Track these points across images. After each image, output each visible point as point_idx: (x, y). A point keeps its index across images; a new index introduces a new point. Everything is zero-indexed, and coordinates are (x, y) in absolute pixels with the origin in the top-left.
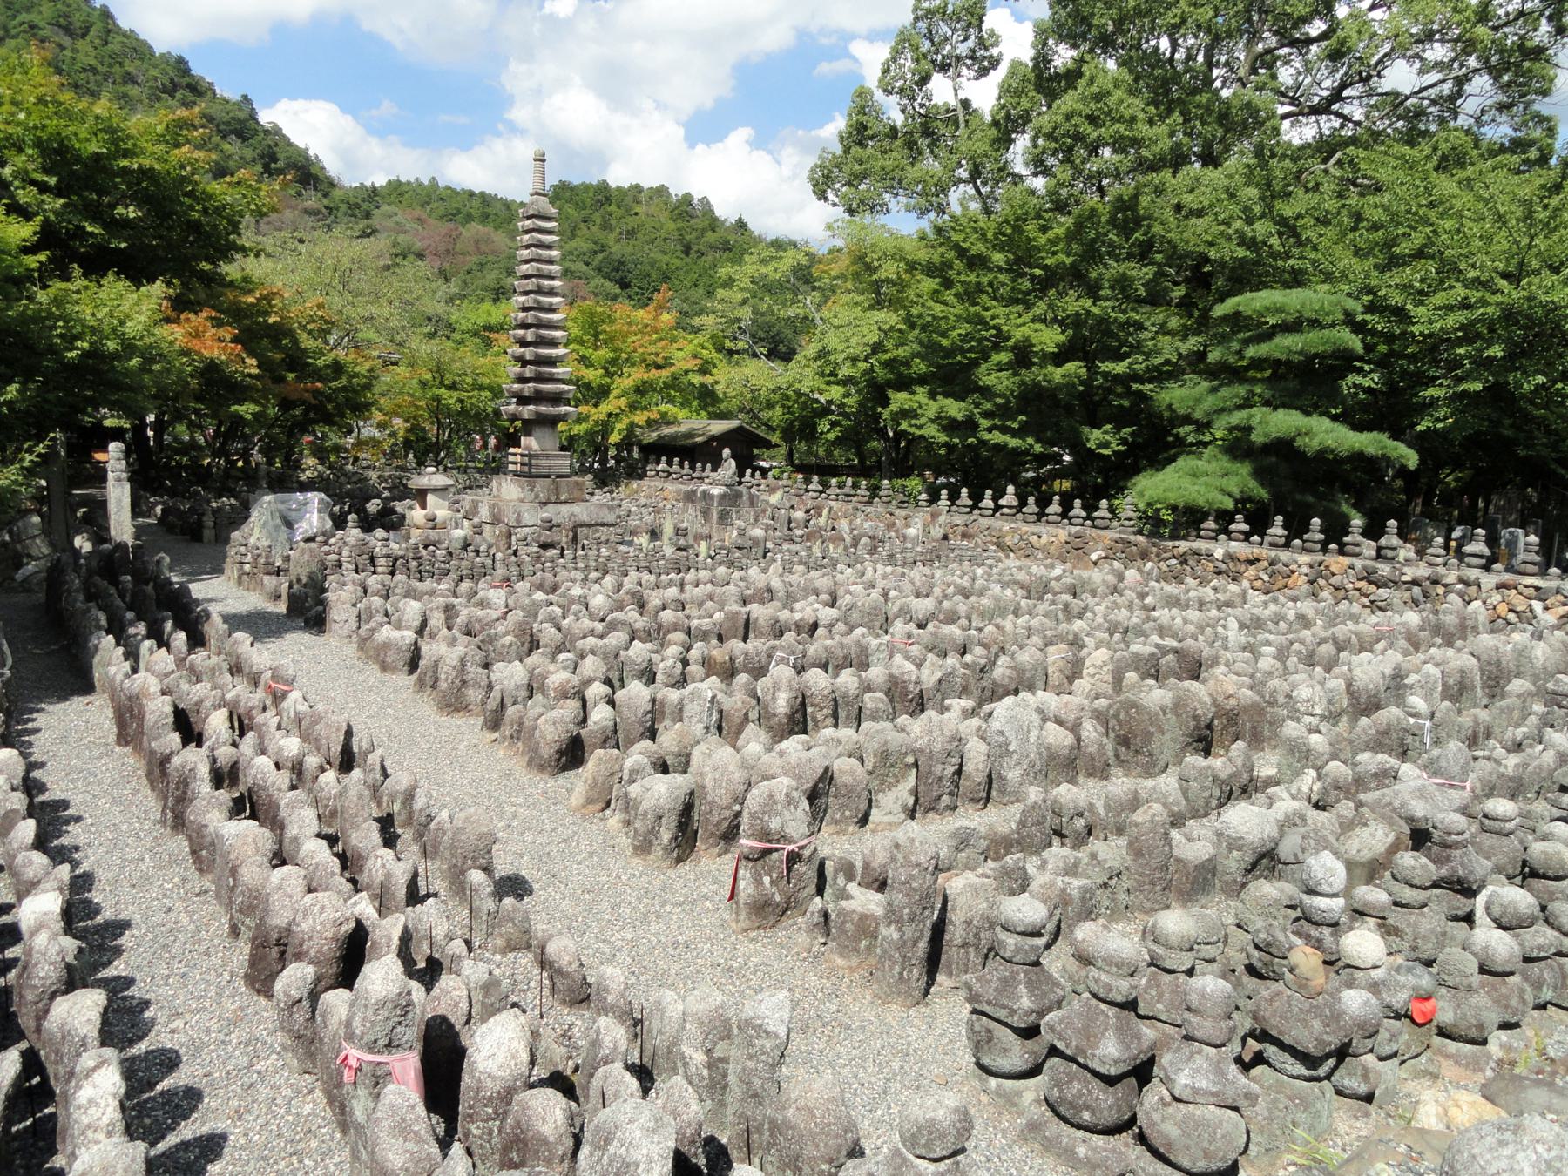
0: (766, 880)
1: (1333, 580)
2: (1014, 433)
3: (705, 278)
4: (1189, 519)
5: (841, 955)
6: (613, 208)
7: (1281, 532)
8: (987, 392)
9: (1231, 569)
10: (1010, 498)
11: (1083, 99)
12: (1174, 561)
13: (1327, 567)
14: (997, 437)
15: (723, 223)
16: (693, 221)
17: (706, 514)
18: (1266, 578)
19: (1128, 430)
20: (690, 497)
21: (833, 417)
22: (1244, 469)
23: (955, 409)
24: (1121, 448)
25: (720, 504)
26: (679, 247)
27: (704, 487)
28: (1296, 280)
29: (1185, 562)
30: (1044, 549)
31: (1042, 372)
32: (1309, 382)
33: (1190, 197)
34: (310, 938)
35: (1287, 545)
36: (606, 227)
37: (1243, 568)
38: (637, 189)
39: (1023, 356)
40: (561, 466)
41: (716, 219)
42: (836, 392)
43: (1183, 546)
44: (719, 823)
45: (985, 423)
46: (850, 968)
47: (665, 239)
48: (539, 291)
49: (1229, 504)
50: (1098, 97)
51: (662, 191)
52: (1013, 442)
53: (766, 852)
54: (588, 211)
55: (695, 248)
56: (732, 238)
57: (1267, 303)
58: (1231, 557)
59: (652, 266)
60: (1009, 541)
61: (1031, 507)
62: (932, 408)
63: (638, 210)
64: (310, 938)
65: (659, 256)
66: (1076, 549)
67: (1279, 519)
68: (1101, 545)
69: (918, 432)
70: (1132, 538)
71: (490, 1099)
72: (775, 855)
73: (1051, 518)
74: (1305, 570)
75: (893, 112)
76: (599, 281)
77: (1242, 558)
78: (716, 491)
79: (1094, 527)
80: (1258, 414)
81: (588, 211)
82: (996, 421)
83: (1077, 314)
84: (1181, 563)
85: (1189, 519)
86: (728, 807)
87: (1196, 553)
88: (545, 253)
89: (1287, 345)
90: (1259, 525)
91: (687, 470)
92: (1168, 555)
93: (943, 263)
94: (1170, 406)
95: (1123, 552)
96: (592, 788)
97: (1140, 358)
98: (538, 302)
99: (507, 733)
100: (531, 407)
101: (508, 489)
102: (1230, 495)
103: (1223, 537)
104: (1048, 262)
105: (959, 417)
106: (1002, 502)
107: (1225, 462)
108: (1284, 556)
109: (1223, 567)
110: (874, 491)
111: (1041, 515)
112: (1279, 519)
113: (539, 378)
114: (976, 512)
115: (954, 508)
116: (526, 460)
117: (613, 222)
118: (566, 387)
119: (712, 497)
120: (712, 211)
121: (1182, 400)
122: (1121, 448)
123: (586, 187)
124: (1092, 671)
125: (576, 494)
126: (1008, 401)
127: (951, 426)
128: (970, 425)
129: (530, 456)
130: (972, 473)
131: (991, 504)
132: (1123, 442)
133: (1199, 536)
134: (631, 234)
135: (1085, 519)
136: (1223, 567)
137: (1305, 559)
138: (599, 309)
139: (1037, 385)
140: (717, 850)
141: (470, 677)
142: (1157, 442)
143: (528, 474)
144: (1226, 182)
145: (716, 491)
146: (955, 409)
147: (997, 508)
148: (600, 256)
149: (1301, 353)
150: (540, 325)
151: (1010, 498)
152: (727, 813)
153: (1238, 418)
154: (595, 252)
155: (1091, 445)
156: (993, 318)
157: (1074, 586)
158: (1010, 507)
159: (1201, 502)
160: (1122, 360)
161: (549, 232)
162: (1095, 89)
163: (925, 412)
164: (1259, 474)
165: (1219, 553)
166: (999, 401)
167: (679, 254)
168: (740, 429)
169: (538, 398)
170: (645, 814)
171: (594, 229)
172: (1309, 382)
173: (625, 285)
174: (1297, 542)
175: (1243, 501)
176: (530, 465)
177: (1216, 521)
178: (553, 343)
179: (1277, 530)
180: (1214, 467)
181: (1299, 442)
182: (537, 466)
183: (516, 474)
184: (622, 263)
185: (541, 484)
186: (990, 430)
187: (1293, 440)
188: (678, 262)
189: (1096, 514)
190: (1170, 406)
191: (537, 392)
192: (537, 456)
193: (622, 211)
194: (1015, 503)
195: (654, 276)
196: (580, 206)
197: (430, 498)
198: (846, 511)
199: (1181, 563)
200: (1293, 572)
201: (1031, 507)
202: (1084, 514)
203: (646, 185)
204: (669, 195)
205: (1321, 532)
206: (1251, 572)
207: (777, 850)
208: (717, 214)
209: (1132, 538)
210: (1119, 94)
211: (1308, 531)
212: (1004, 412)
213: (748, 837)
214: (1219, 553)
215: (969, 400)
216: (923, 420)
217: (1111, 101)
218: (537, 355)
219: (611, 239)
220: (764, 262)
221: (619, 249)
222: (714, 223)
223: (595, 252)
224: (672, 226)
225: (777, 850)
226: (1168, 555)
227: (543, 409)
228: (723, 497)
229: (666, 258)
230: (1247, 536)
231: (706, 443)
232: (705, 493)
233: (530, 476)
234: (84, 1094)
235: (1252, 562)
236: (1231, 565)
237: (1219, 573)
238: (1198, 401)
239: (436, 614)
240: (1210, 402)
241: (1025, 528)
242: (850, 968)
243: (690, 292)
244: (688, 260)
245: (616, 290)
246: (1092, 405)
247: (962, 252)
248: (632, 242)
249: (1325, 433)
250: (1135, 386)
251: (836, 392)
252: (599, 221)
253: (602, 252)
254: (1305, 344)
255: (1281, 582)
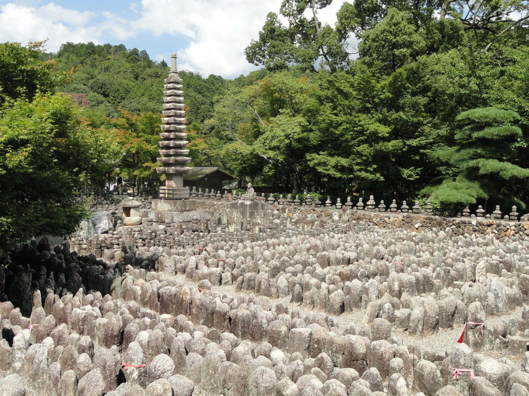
0: (476, 335)
1: (526, 232)
2: (371, 173)
3: (148, 91)
4: (451, 209)
5: (513, 355)
6: (96, 56)
7: (499, 212)
8: (359, 154)
9: (480, 229)
10: (371, 201)
11: (389, 24)
12: (454, 227)
13: (523, 227)
14: (363, 174)
15: (154, 63)
16: (139, 63)
17: (243, 213)
18: (496, 232)
19: (420, 169)
20: (234, 206)
21: (270, 165)
22: (476, 185)
23: (344, 162)
24: (418, 177)
25: (250, 209)
26: (132, 76)
27: (240, 201)
28: (485, 103)
29: (460, 227)
30: (393, 224)
31: (368, 141)
32: (499, 147)
33: (437, 67)
34: (385, 353)
35: (502, 218)
36: (93, 66)
37: (486, 228)
38: (108, 46)
39: (374, 138)
40: (186, 194)
41: (151, 61)
42: (271, 154)
43: (458, 220)
44: (432, 323)
45: (356, 168)
46: (517, 358)
47: (125, 72)
48: (176, 115)
49: (474, 201)
50: (395, 25)
51: (121, 48)
52: (371, 177)
53: (476, 325)
54: (83, 58)
55: (141, 76)
56: (159, 71)
57: (481, 114)
58: (479, 224)
59: (120, 85)
60: (375, 220)
61: (382, 205)
62: (333, 161)
63: (109, 57)
64: (385, 353)
65: (123, 81)
66: (407, 223)
67: (498, 207)
68: (419, 221)
69: (327, 172)
70: (434, 217)
71: (495, 380)
72: (478, 327)
73: (392, 209)
74: (513, 228)
75: (285, 23)
76: (91, 94)
77: (485, 224)
78: (248, 203)
79: (413, 212)
80: (481, 162)
81: (83, 58)
82: (363, 167)
83: (396, 119)
84: (457, 227)
85: (451, 209)
86: (435, 317)
87: (464, 223)
88: (178, 99)
89: (489, 132)
90: (489, 210)
91: (200, 192)
92: (451, 224)
93: (333, 96)
94: (438, 158)
95: (427, 224)
96: (370, 316)
97: (424, 138)
98: (175, 120)
99: (308, 302)
100: (173, 168)
101: (162, 206)
102: (473, 197)
103: (473, 215)
104: (382, 96)
105: (346, 165)
106: (368, 203)
107: (466, 183)
108: (503, 222)
109: (477, 228)
110: (276, 199)
111: (387, 208)
112: (498, 207)
113: (176, 155)
114: (355, 208)
115: (344, 206)
116: (171, 192)
117: (97, 63)
118: (188, 158)
119: (246, 205)
120: (148, 57)
121: (444, 156)
122: (418, 177)
123: (82, 46)
124: (479, 271)
125: (193, 207)
126: (368, 158)
127: (342, 169)
128: (350, 170)
129: (173, 190)
130: (334, 190)
131: (362, 204)
132: (417, 174)
133: (462, 215)
134: (107, 69)
135: (408, 210)
136: (477, 228)
137: (512, 223)
138: (154, 116)
139: (381, 151)
140: (431, 333)
141: (271, 283)
142: (432, 175)
143: (171, 198)
144: (451, 60)
145: (248, 203)
146: (344, 162)
147: (365, 205)
148: (91, 81)
149: (497, 135)
150: (176, 131)
151: (371, 201)
152: (434, 319)
153: (472, 163)
154: (89, 79)
155: (405, 176)
156: (359, 121)
157: (422, 239)
158: (372, 205)
159: (463, 200)
160: (415, 138)
161: (178, 89)
162: (394, 21)
163: (326, 163)
164: (482, 187)
165: (474, 222)
166: (364, 158)
167: (132, 79)
168: (217, 172)
169: (177, 163)
170: (414, 320)
171: (87, 67)
172: (499, 147)
173: (106, 96)
174: (507, 216)
175: (480, 201)
176: (173, 194)
177: (469, 208)
178: (181, 139)
179: (498, 211)
180: (462, 185)
181: (501, 173)
182: (176, 194)
183: (165, 199)
184: (104, 85)
185: (179, 202)
186: (360, 170)
187: (499, 172)
188: (132, 84)
189: (414, 207)
190: (438, 158)
191: (176, 161)
192: (176, 190)
193: (101, 58)
194: (374, 203)
195: (121, 91)
196: (78, 55)
197: (132, 211)
198: (281, 210)
199: (457, 227)
200: (508, 229)
201: (382, 205)
202: (408, 207)
203: (113, 44)
204: (125, 50)
205: (517, 212)
206: (489, 230)
207: (479, 325)
208: (151, 59)
209: (434, 217)
210: (404, 23)
211: (511, 211)
212: (366, 163)
213: (471, 321)
214: (474, 222)
215: (351, 158)
216: (329, 167)
217: (402, 25)
218: (175, 144)
219: (96, 72)
220: (235, 93)
221: (102, 77)
222: (150, 64)
223: (89, 79)
224: (128, 65)
225: (479, 325)
226: (451, 224)
227: (178, 168)
228: (251, 205)
229: (126, 82)
230: (484, 215)
231: (202, 178)
232: (242, 204)
233: (173, 199)
234: (399, 384)
235: (489, 225)
236: (480, 227)
237: (475, 231)
238: (451, 156)
239: (201, 262)
240: (456, 156)
241: (382, 214)
242: (517, 358)
243: (141, 99)
244: (137, 82)
245: (101, 98)
246: (404, 158)
247: (340, 91)
248: (108, 73)
249: (511, 170)
250: (422, 151)
251: (271, 154)
252: (89, 63)
253: (92, 78)
254: (499, 131)
255: (503, 234)
